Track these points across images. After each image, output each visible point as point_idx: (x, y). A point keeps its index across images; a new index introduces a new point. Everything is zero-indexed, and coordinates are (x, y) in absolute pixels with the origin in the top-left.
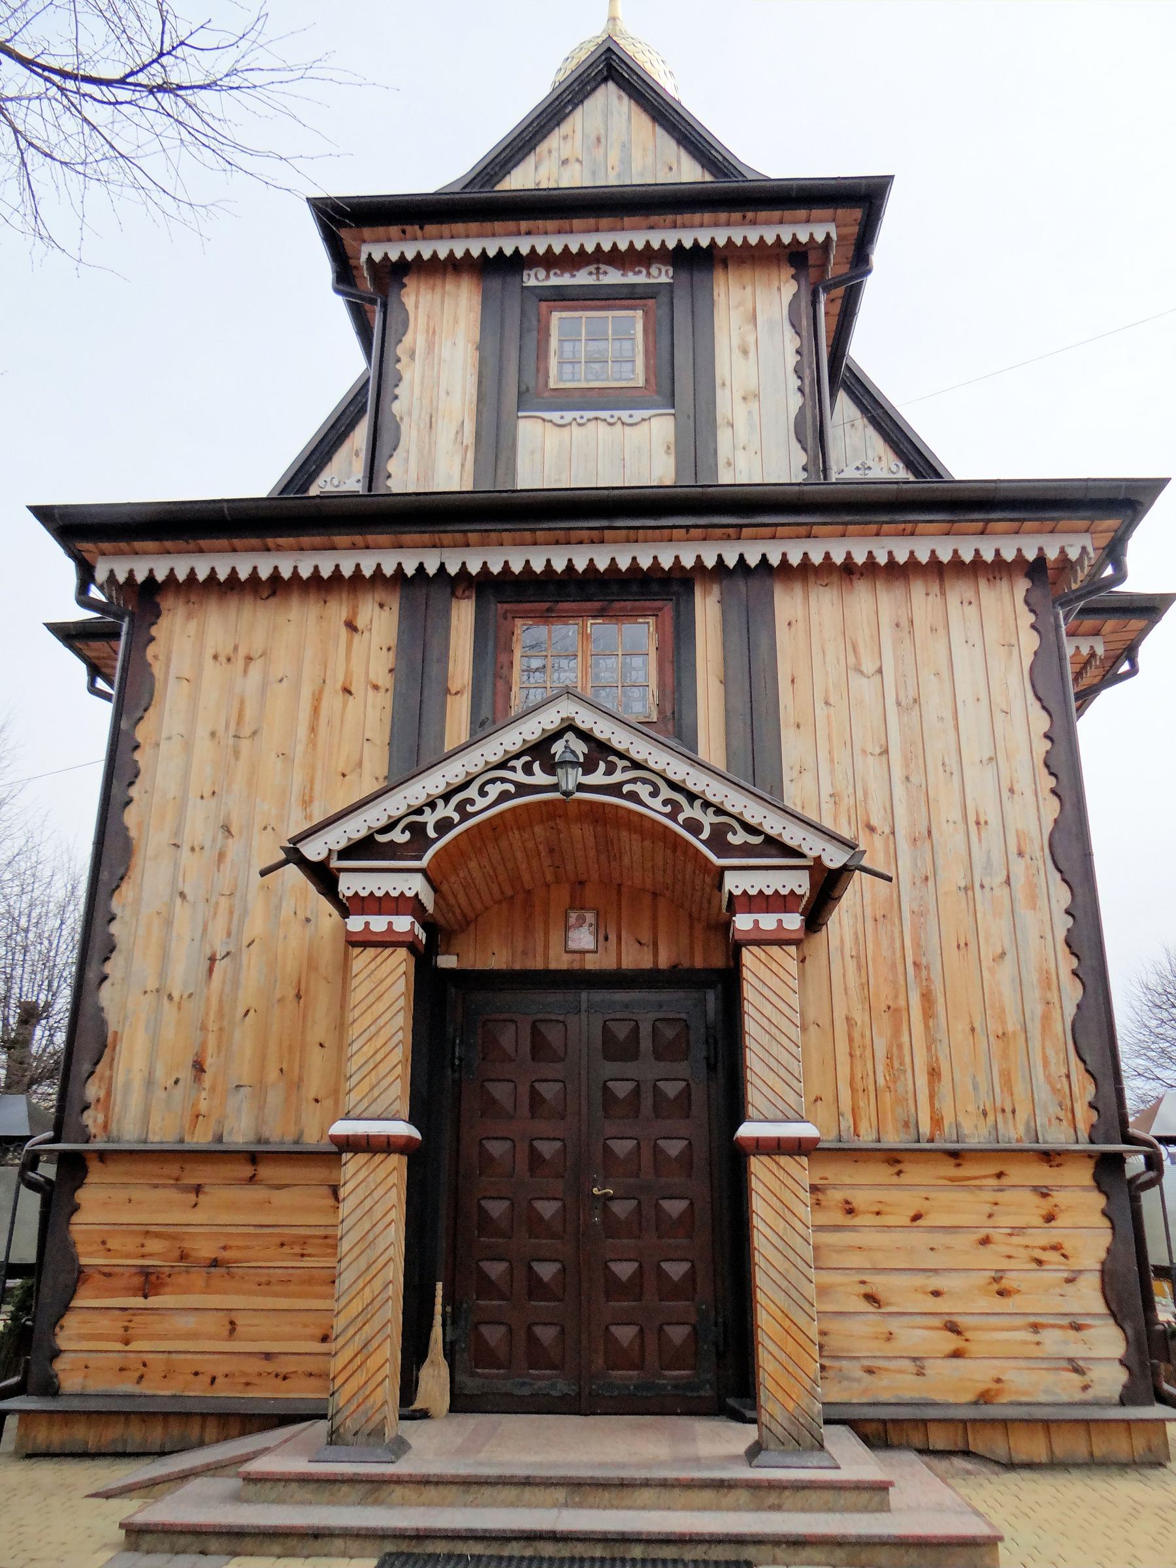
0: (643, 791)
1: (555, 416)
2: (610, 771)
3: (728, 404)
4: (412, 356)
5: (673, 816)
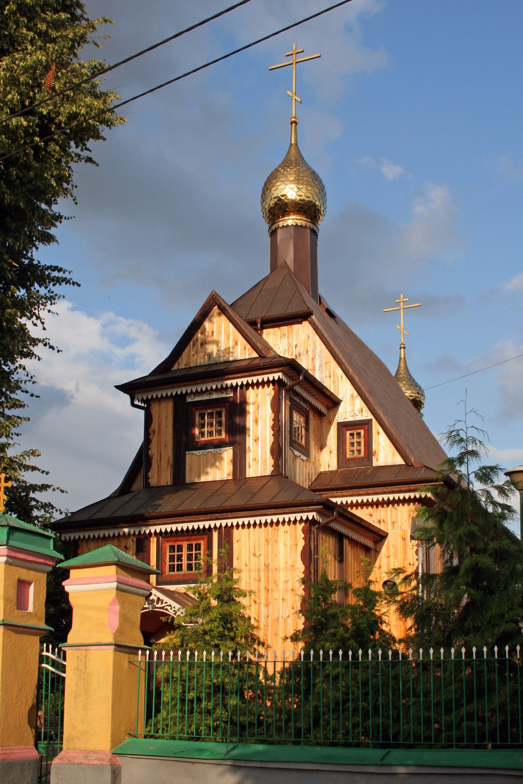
0: (169, 608)
2: (162, 604)
3: (250, 442)
4: (154, 433)
5: (175, 614)
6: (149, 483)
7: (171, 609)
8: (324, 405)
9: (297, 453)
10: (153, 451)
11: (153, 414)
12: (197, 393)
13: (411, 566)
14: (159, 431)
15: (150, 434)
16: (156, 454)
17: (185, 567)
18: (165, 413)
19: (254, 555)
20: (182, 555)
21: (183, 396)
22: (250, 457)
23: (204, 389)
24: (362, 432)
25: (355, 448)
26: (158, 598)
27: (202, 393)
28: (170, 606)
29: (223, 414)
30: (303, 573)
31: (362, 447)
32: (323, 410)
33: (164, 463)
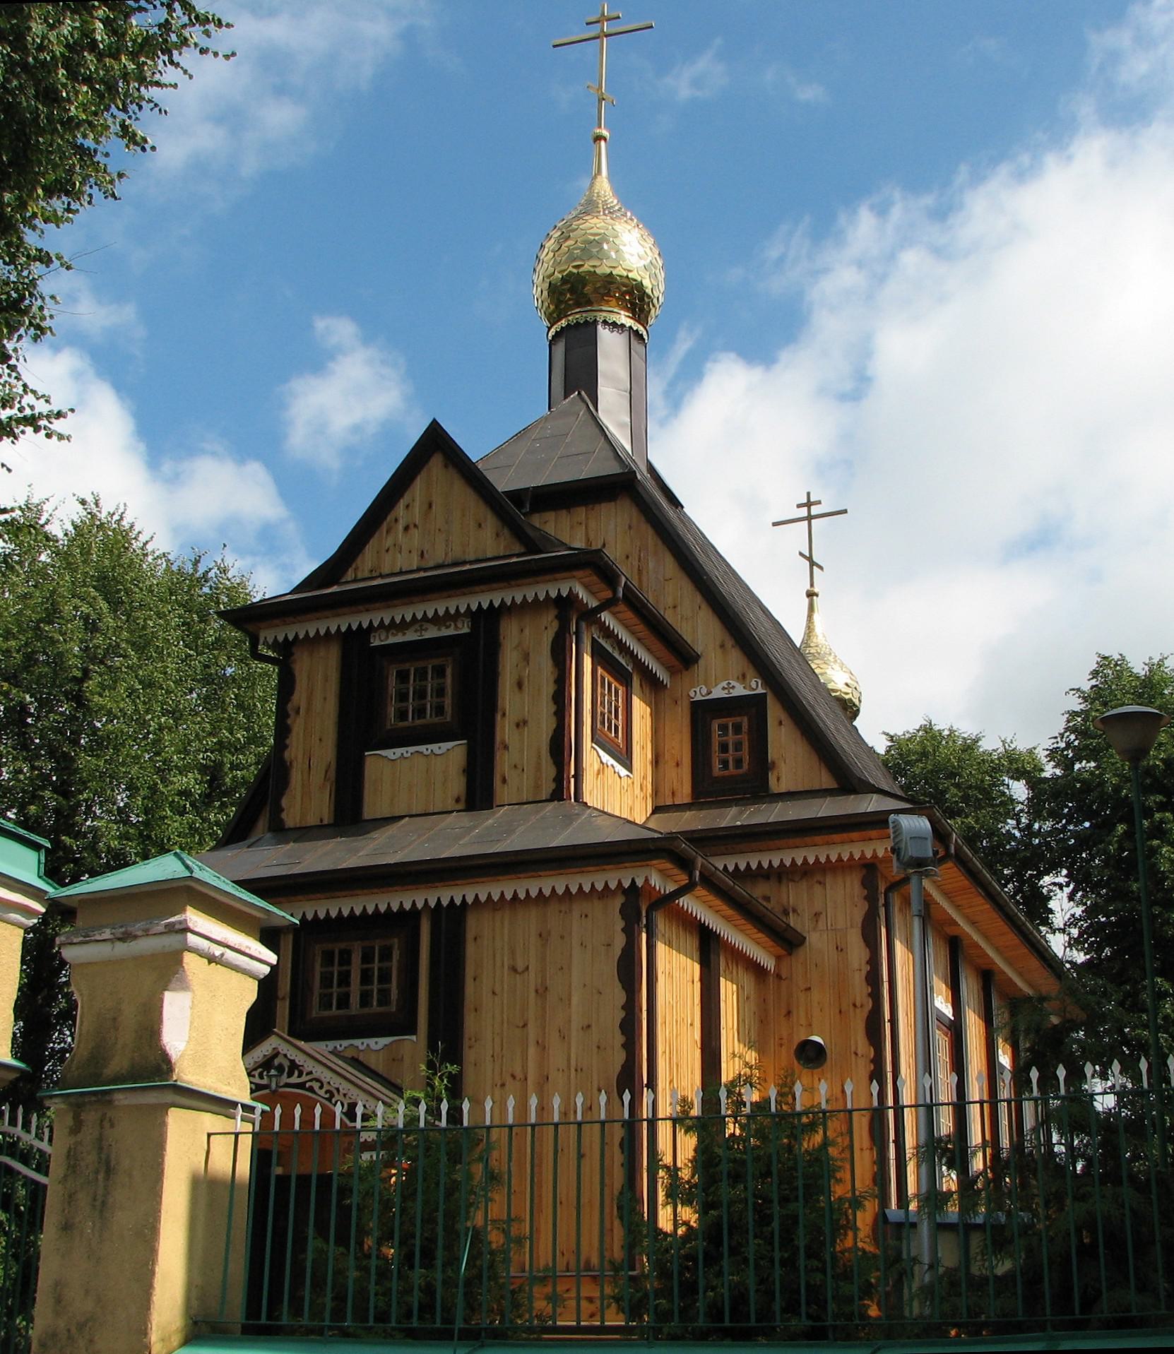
0: (316, 1085)
1: (388, 753)
2: (299, 1076)
3: (505, 730)
4: (298, 712)
6: (282, 821)
7: (321, 1087)
8: (663, 664)
9: (606, 758)
10: (295, 752)
11: (297, 674)
12: (393, 627)
13: (858, 1011)
14: (308, 710)
15: (288, 716)
16: (300, 760)
17: (355, 999)
18: (320, 680)
19: (514, 969)
20: (348, 973)
21: (363, 634)
22: (504, 763)
23: (408, 618)
24: (745, 721)
25: (730, 756)
26: (292, 1062)
27: (403, 626)
28: (317, 1080)
29: (449, 671)
30: (623, 1008)
31: (745, 754)
32: (662, 674)
33: (317, 777)
